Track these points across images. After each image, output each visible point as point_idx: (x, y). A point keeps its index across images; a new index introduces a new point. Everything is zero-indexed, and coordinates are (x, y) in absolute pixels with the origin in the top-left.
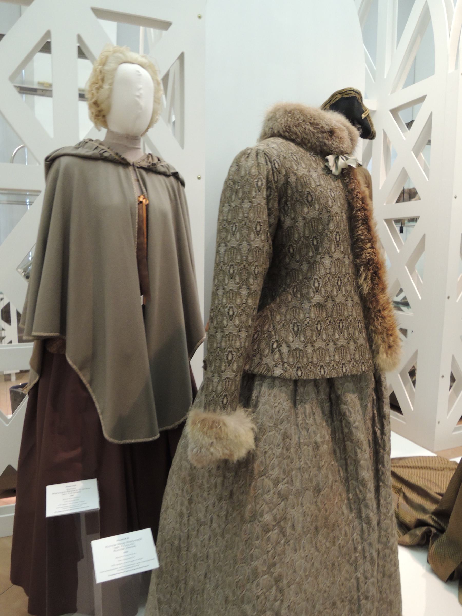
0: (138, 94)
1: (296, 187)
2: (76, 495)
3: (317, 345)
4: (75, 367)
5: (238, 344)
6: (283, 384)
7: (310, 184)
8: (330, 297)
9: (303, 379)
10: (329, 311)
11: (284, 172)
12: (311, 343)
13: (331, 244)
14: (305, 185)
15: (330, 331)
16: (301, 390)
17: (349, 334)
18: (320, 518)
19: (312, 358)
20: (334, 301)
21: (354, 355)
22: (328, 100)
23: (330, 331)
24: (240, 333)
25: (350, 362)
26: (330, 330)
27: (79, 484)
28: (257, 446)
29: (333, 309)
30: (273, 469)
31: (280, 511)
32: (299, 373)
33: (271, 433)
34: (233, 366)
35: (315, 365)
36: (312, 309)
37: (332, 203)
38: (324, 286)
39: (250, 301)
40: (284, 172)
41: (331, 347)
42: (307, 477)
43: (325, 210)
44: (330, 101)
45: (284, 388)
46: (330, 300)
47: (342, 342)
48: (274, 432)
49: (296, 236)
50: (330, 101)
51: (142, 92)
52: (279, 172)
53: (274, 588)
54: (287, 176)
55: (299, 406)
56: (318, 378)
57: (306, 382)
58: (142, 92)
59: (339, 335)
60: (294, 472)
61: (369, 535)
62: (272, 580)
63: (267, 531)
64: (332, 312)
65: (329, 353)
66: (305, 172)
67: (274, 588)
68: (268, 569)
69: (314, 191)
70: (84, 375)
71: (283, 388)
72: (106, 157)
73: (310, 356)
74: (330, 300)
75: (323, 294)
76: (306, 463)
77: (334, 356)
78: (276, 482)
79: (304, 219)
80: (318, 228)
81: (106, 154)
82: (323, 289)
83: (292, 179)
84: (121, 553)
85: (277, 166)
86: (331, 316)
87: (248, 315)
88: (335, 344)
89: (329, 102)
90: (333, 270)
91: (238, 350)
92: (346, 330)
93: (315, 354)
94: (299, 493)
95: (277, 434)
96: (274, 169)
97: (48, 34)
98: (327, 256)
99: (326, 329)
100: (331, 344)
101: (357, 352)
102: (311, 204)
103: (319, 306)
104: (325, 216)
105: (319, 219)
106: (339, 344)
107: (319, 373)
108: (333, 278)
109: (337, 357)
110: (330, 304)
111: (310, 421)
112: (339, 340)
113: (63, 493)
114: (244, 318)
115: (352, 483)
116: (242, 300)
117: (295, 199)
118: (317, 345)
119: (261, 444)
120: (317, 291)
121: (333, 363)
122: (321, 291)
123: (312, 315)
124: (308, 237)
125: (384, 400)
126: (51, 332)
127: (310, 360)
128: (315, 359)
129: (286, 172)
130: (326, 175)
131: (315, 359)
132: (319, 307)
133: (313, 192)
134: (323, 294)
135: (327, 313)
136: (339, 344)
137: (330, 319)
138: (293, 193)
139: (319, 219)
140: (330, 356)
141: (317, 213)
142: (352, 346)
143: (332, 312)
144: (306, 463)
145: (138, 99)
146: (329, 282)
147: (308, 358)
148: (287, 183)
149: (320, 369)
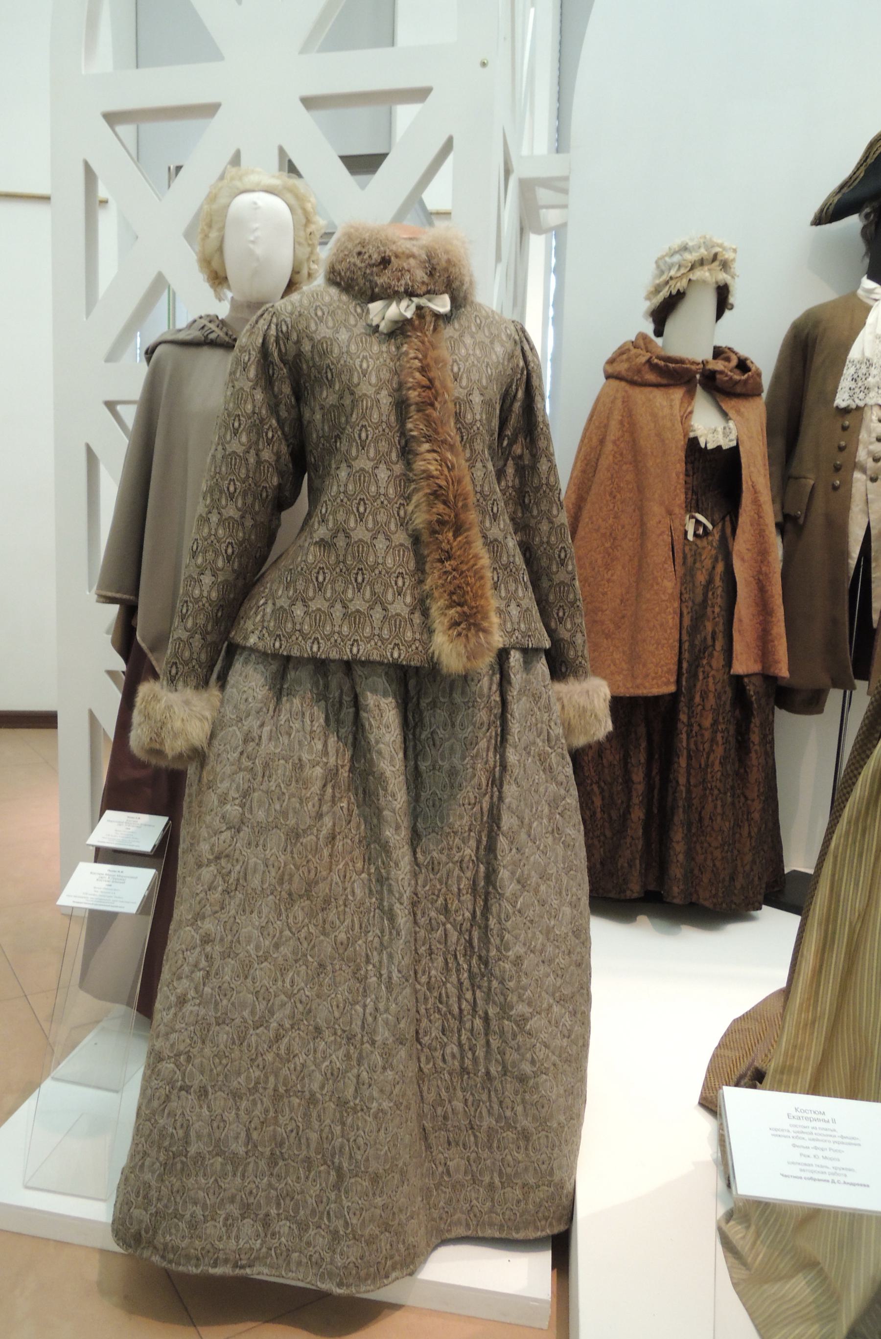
0: (252, 238)
1: (313, 358)
2: (132, 829)
3: (313, 606)
4: (143, 645)
5: (197, 592)
6: (260, 660)
7: (332, 352)
8: (342, 530)
9: (282, 655)
10: (341, 552)
11: (294, 337)
12: (303, 601)
13: (351, 446)
14: (324, 354)
15: (339, 587)
16: (292, 675)
17: (373, 593)
18: (296, 879)
19: (302, 624)
20: (348, 536)
21: (381, 629)
22: (863, 156)
23: (339, 587)
24: (202, 577)
25: (369, 639)
26: (340, 583)
27: (144, 818)
28: (210, 744)
29: (346, 550)
30: (222, 781)
31: (221, 842)
32: (277, 645)
33: (231, 729)
34: (187, 622)
35: (305, 637)
36: (312, 548)
37: (359, 378)
38: (335, 513)
39: (221, 532)
40: (294, 337)
41: (338, 611)
42: (278, 807)
43: (347, 392)
44: (867, 158)
45: (261, 667)
46: (341, 535)
47: (358, 604)
48: (235, 728)
49: (314, 436)
50: (867, 158)
51: (258, 233)
52: (287, 337)
53: (198, 949)
54: (298, 342)
55: (284, 699)
56: (306, 655)
57: (300, 662)
58: (258, 233)
59: (354, 593)
60: (256, 794)
61: (391, 940)
62: (198, 937)
63: (200, 866)
64: (345, 556)
65: (332, 620)
66: (329, 333)
67: (198, 949)
68: (192, 918)
69: (335, 362)
70: (157, 660)
71: (261, 666)
72: (212, 341)
73: (298, 620)
74: (341, 535)
75: (331, 525)
76: (279, 786)
77: (340, 626)
78: (223, 800)
79: (322, 408)
80: (339, 422)
81: (212, 336)
82: (331, 517)
83: (307, 347)
84: (103, 885)
85: (284, 329)
86: (344, 562)
87: (217, 553)
88: (345, 607)
89: (865, 161)
90: (351, 487)
91: (197, 600)
92: (368, 588)
93: (308, 618)
94: (262, 829)
95: (238, 733)
96: (280, 334)
97: (282, 151)
98: (344, 465)
99: (333, 581)
100: (338, 606)
101: (386, 625)
102: (331, 384)
103: (323, 544)
104: (347, 401)
105: (339, 407)
106: (352, 608)
107: (310, 649)
108: (349, 500)
109: (345, 629)
110: (341, 542)
111: (296, 725)
112: (352, 600)
113: (120, 823)
114: (210, 556)
115: (375, 848)
116: (210, 529)
117: (313, 378)
118: (313, 606)
119: (216, 742)
120: (323, 521)
121: (336, 636)
122: (328, 521)
123: (311, 558)
124: (328, 437)
125: (509, 737)
126: (118, 592)
127: (298, 627)
128: (306, 627)
129: (298, 336)
130: (370, 335)
131: (306, 627)
132: (324, 546)
133: (333, 364)
134: (331, 525)
135: (337, 556)
136: (352, 608)
137: (341, 565)
138: (309, 368)
139: (339, 407)
140: (333, 625)
141: (336, 396)
142: (377, 614)
143: (345, 556)
144: (279, 786)
145: (251, 246)
146: (343, 506)
147: (294, 624)
148: (299, 355)
149: (313, 643)
